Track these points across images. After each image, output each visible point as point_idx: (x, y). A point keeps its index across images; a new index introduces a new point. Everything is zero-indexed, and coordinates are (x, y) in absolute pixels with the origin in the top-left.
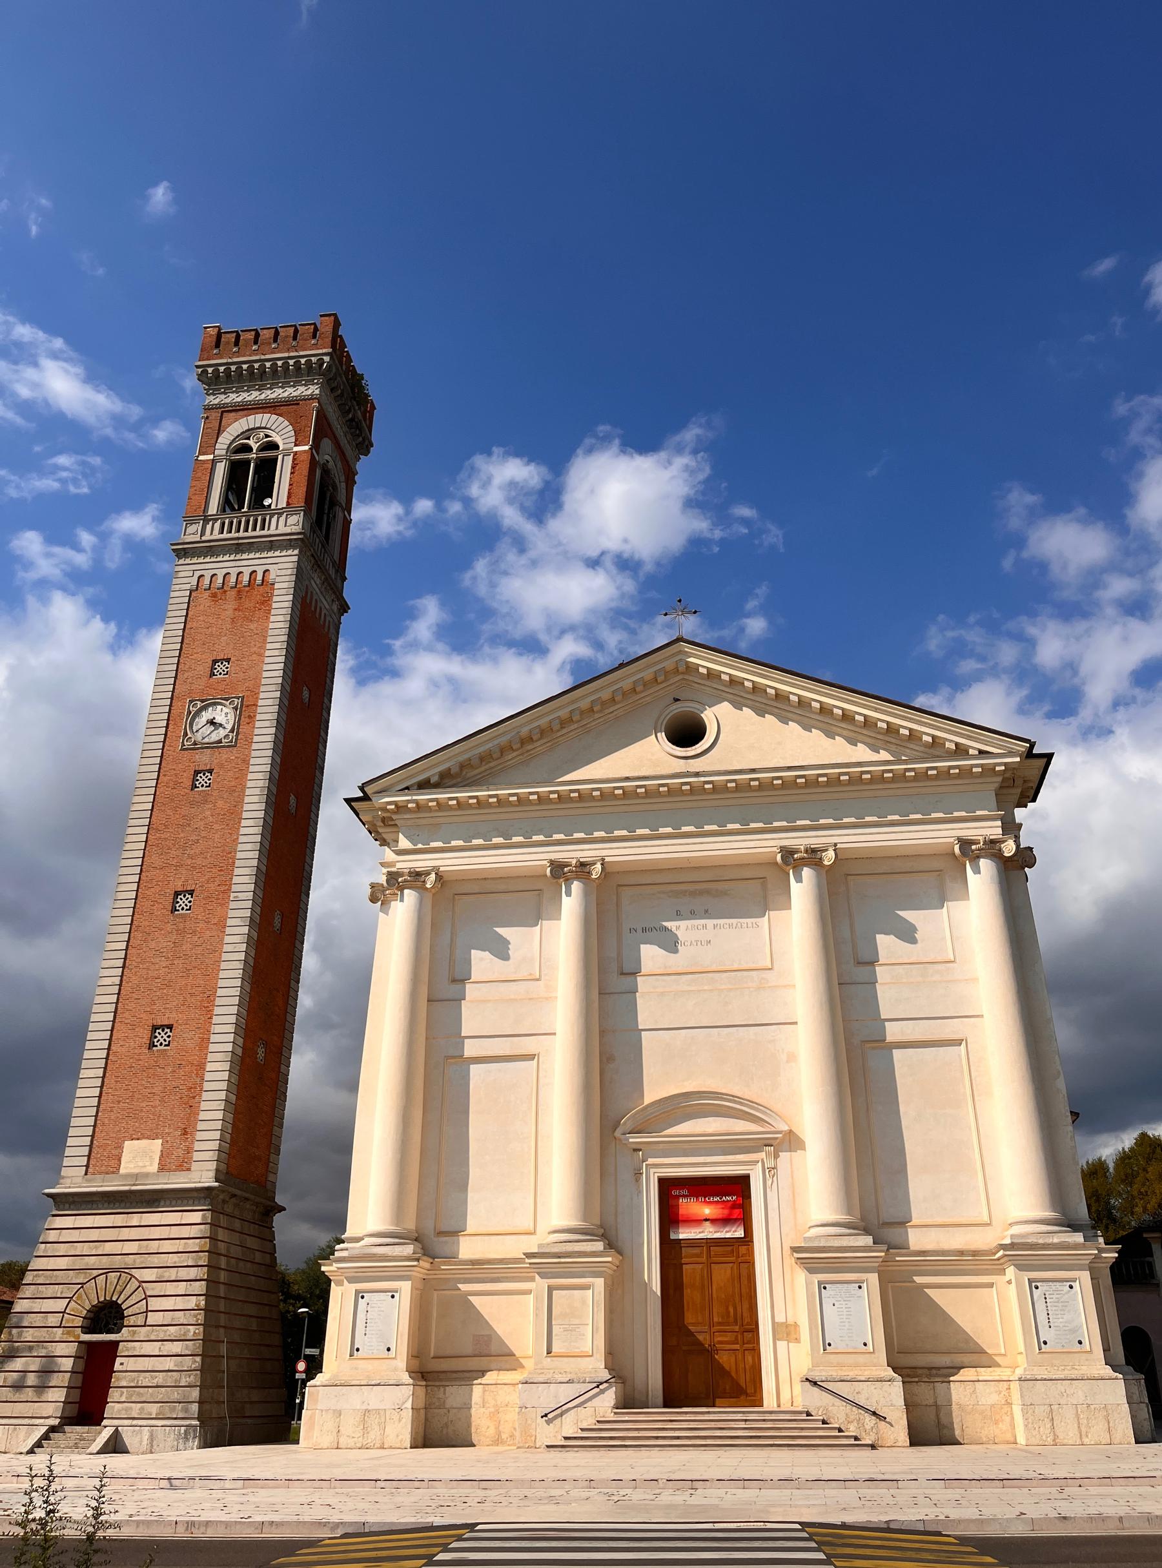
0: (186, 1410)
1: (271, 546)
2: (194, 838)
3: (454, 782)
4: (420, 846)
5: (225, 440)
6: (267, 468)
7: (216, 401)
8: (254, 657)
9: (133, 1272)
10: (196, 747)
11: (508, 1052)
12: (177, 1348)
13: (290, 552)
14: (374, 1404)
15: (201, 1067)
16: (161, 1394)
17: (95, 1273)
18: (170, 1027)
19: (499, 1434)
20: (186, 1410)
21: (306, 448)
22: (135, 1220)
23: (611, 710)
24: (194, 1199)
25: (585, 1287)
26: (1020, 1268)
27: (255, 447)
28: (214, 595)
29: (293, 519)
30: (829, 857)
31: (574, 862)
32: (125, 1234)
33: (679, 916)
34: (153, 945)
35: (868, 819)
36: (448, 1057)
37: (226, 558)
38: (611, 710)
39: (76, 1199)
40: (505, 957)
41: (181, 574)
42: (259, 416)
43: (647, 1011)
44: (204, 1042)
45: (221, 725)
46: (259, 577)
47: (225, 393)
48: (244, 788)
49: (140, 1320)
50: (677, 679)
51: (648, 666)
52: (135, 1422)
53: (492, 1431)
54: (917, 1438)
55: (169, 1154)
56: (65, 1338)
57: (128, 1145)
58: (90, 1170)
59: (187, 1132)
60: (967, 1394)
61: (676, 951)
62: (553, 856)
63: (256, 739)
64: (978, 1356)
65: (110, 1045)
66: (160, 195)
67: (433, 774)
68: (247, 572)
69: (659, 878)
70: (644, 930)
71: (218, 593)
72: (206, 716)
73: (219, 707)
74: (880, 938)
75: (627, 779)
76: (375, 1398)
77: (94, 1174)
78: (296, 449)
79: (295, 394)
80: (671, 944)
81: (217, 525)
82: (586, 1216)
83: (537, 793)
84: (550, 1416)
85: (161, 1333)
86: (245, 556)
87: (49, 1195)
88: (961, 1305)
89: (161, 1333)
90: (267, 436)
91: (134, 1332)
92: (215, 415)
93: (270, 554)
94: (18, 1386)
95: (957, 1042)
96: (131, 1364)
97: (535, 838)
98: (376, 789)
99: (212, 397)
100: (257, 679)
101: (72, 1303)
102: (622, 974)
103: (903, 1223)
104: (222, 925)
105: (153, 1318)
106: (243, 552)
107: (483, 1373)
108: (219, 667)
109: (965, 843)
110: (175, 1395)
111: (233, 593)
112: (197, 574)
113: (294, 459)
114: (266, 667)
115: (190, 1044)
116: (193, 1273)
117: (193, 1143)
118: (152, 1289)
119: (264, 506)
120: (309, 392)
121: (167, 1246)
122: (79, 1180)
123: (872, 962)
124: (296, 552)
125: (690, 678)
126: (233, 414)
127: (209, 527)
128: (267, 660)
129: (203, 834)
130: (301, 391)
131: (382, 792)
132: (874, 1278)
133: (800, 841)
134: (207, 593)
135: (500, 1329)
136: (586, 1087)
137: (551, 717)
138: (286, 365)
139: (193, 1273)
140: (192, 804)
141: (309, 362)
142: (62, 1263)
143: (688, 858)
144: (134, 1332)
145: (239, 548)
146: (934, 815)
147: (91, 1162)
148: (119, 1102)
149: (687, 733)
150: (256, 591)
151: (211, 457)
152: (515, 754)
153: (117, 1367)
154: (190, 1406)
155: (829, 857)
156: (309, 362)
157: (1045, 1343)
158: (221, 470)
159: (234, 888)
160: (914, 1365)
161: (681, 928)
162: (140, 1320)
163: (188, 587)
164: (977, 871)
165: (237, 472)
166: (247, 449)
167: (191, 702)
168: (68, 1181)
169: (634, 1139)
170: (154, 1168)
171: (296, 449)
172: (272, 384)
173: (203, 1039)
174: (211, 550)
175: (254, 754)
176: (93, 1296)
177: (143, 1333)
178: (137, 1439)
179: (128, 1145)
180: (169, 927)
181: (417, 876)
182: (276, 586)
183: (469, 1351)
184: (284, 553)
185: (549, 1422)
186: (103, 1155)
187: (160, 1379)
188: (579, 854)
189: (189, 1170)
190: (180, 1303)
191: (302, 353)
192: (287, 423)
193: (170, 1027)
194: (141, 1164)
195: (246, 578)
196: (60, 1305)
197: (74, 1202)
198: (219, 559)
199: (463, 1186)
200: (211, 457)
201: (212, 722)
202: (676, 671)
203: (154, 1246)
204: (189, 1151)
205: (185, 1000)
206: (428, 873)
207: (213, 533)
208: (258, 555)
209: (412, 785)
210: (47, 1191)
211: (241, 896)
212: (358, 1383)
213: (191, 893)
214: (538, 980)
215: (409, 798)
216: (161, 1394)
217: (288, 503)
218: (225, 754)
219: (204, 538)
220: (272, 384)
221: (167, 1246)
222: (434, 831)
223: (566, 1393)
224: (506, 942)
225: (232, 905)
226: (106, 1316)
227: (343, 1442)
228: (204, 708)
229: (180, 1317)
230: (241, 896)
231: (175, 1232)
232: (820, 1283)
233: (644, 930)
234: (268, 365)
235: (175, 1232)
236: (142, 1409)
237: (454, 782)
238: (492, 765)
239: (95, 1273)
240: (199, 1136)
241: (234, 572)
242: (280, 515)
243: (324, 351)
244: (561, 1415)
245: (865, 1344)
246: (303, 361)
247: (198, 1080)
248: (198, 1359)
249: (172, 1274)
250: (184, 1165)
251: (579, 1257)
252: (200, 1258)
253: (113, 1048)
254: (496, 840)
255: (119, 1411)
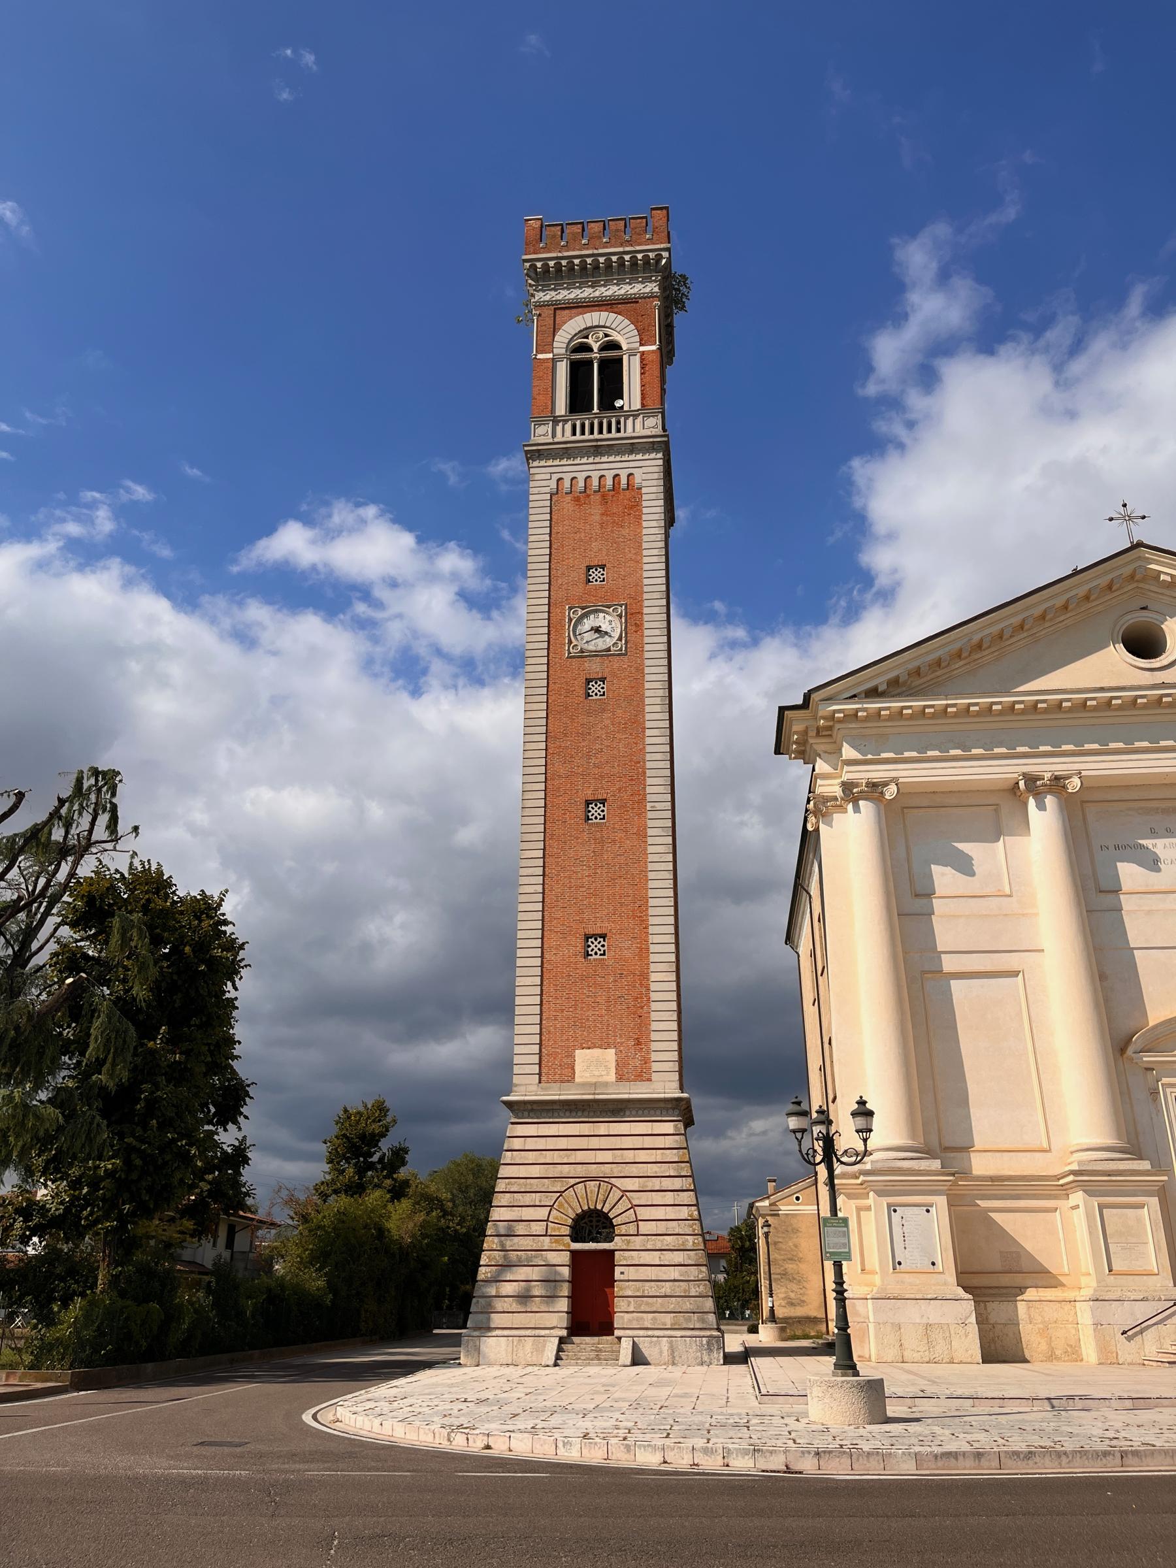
0: (703, 1321)
1: (633, 448)
2: (598, 746)
3: (899, 690)
4: (870, 756)
5: (562, 339)
6: (612, 370)
7: (547, 298)
8: (631, 564)
9: (613, 1181)
10: (583, 655)
11: (989, 968)
12: (678, 1257)
13: (653, 456)
14: (934, 1318)
15: (644, 976)
16: (672, 1304)
17: (573, 1181)
18: (604, 936)
19: (1053, 1350)
20: (703, 1321)
21: (654, 348)
22: (603, 1129)
23: (1062, 618)
24: (661, 1109)
25: (1142, 1206)
26: (1090, 1193)
27: (595, 347)
28: (577, 499)
29: (651, 422)
30: (1074, 784)
31: (1047, 776)
32: (595, 1143)
33: (1153, 833)
34: (572, 853)
35: (1064, 747)
36: (924, 972)
37: (584, 460)
38: (1062, 618)
39: (535, 1107)
40: (971, 873)
41: (537, 477)
42: (596, 315)
43: (1137, 930)
44: (643, 952)
45: (606, 633)
46: (624, 481)
47: (555, 290)
48: (642, 698)
49: (632, 1229)
50: (1130, 587)
51: (1106, 573)
52: (650, 1333)
53: (1044, 1346)
54: (989, 1357)
55: (626, 1065)
56: (554, 1246)
57: (579, 1054)
58: (543, 1079)
59: (641, 1041)
60: (1031, 1313)
61: (1159, 870)
62: (1026, 769)
63: (647, 647)
64: (1045, 1277)
65: (542, 953)
66: (285, 96)
67: (881, 682)
68: (609, 475)
69: (1125, 795)
70: (1117, 847)
71: (582, 497)
72: (588, 623)
73: (601, 615)
74: (935, 868)
75: (1102, 689)
76: (934, 1313)
77: (548, 1082)
78: (642, 349)
79: (632, 291)
80: (1152, 863)
81: (568, 427)
82: (913, 1134)
83: (1000, 703)
84: (1130, 1333)
85: (659, 1242)
86: (604, 459)
87: (505, 1103)
88: (1024, 1227)
89: (659, 1242)
90: (606, 335)
91: (629, 1242)
92: (548, 312)
93: (632, 457)
94: (524, 1297)
95: (1015, 974)
96: (631, 1273)
97: (996, 750)
98: (822, 697)
99: (541, 294)
100: (639, 585)
101: (554, 1212)
102: (916, 895)
103: (966, 1149)
104: (642, 835)
105: (645, 1228)
106: (602, 455)
107: (1022, 1290)
108: (595, 574)
109: (1031, 779)
110: (688, 1305)
111: (598, 497)
112: (555, 477)
113: (642, 360)
114: (645, 574)
115: (627, 954)
116: (678, 1183)
117: (648, 1053)
118: (637, 1199)
119: (614, 408)
120: (647, 290)
121: (643, 1156)
122: (534, 1088)
123: (1116, 891)
124: (660, 455)
125: (1147, 587)
126: (567, 311)
127: (559, 428)
128: (646, 567)
129: (606, 743)
130: (637, 289)
131: (829, 699)
132: (941, 1201)
133: (1046, 768)
134: (569, 498)
135: (1030, 1245)
136: (1097, 1005)
137: (1002, 625)
138: (621, 262)
139: (678, 1183)
140: (589, 714)
141: (646, 258)
142: (535, 1171)
143: (1167, 774)
144: (629, 1242)
145: (597, 450)
146: (1042, 748)
147: (544, 1071)
148: (562, 1011)
149: (1144, 644)
150: (624, 497)
151: (550, 356)
152: (961, 663)
153: (617, 1276)
154: (706, 1316)
155: (891, 792)
156: (646, 258)
157: (900, 1263)
158: (563, 370)
159: (649, 798)
160: (977, 1285)
161: (1160, 846)
162: (632, 1229)
163: (547, 490)
164: (1041, 807)
165: (579, 372)
166: (587, 348)
167: (570, 609)
168: (522, 1088)
169: (1148, 1058)
170: (612, 1077)
171: (642, 349)
172: (595, 282)
173: (641, 949)
174: (567, 452)
175: (647, 663)
176: (575, 1204)
177: (637, 1242)
178: (656, 1350)
179: (579, 1054)
180: (585, 836)
181: (875, 789)
182: (644, 490)
183: (999, 1268)
184: (646, 457)
185: (1129, 1339)
186: (552, 1063)
187: (667, 1288)
188: (1053, 768)
189: (650, 1080)
190: (671, 1213)
191: (638, 248)
192: (627, 322)
193: (604, 936)
194: (597, 1073)
195: (609, 482)
196: (542, 1213)
197: (532, 1110)
198: (578, 461)
199: (964, 1102)
200: (550, 356)
201: (597, 630)
202: (1132, 577)
203: (629, 1156)
204: (646, 1061)
205: (615, 909)
206: (886, 784)
207: (564, 433)
208: (618, 458)
209: (860, 693)
210: (505, 1098)
211: (659, 806)
212: (912, 1296)
213: (603, 802)
214: (1010, 896)
215: (859, 706)
216: (672, 1304)
217: (643, 405)
218: (616, 663)
219: (556, 440)
220: (595, 282)
221: (643, 1156)
222: (882, 742)
223: (1142, 1311)
224: (970, 859)
225: (650, 815)
226: (592, 1224)
227: (908, 1355)
228: (586, 615)
229: (674, 1227)
230: (659, 806)
231: (648, 1142)
232: (889, 1206)
233: (1117, 847)
234: (602, 260)
235: (648, 1142)
236: (654, 1319)
237: (899, 690)
238: (938, 673)
239: (573, 1181)
240: (654, 1046)
241: (595, 476)
242: (635, 417)
243: (662, 246)
244: (1141, 1332)
245: (933, 1264)
246: (640, 256)
247: (644, 990)
248: (704, 1269)
249: (656, 1184)
250: (643, 1074)
251: (1132, 1175)
252: (682, 1168)
253: (546, 956)
254: (953, 752)
255: (630, 1321)
